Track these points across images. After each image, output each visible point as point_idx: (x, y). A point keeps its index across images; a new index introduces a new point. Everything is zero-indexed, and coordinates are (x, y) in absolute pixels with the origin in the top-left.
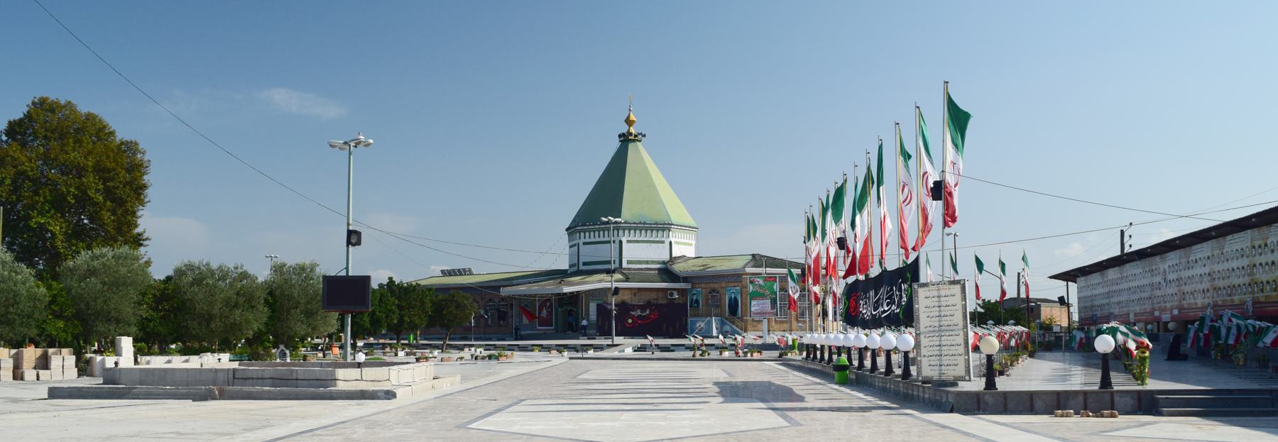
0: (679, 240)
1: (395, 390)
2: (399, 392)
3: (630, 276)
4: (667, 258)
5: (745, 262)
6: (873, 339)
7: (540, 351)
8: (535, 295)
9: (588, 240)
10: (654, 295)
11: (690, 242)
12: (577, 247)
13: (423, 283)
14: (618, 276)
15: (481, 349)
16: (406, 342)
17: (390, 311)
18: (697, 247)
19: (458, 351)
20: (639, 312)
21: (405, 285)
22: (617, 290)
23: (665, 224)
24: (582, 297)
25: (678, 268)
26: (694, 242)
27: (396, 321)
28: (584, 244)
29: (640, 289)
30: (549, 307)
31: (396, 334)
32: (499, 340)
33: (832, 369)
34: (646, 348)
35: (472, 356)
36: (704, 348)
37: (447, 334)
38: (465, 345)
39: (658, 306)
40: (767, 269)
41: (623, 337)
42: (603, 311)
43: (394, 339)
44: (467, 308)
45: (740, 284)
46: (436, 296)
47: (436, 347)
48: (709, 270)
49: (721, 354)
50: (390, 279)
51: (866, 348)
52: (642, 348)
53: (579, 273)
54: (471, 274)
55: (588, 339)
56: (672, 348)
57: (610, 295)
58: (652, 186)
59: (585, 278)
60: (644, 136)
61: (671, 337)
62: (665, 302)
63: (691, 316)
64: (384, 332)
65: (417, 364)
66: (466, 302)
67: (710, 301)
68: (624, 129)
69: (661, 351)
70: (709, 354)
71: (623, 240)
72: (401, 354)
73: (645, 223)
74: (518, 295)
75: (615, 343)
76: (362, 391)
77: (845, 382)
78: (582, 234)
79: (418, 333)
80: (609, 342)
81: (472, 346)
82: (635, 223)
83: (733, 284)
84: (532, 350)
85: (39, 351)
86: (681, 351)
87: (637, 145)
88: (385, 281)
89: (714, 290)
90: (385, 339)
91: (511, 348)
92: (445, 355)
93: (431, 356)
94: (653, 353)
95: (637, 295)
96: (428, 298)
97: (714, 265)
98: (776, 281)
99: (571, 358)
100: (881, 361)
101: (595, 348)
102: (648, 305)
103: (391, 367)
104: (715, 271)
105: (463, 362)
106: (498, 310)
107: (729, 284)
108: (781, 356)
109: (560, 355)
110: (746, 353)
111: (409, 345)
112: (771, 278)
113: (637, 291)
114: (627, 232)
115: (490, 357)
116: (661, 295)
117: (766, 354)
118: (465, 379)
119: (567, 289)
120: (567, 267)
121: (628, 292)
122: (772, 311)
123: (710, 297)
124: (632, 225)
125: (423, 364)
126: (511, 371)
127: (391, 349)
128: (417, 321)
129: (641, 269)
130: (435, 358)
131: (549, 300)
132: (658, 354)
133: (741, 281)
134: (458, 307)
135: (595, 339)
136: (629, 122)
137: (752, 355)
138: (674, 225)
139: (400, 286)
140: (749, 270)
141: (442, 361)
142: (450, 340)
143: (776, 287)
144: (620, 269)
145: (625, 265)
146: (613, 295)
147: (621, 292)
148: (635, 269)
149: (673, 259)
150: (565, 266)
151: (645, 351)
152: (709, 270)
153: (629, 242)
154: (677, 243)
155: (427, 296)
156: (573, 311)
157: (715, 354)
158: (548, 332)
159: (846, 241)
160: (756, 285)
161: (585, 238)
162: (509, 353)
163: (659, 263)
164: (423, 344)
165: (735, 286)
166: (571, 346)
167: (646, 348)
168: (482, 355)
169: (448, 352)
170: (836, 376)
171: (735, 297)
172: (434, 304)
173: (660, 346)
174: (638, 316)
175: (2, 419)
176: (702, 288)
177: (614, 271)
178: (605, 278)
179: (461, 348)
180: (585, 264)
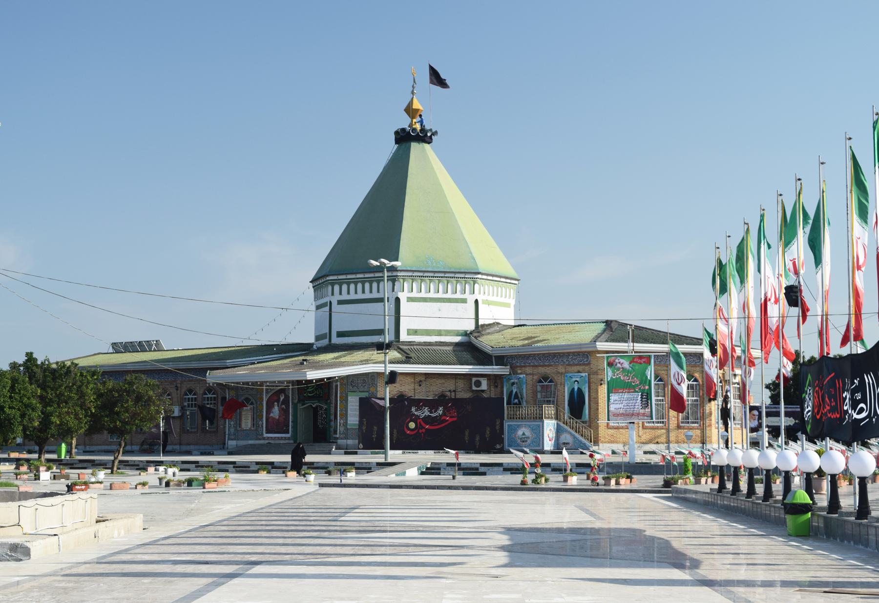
0: (490, 298)
1: (28, 544)
2: (36, 548)
3: (412, 355)
4: (470, 326)
5: (595, 334)
6: (831, 459)
7: (269, 472)
8: (262, 384)
9: (345, 297)
10: (450, 385)
11: (507, 300)
12: (327, 308)
13: (82, 363)
14: (393, 354)
15: (176, 470)
16: (54, 456)
17: (27, 406)
18: (518, 308)
19: (138, 472)
20: (426, 412)
21: (54, 366)
22: (393, 377)
24: (337, 386)
25: (487, 342)
26: (512, 302)
27: (36, 424)
28: (340, 302)
29: (428, 376)
30: (283, 403)
31: (37, 444)
32: (202, 454)
33: (782, 512)
34: (439, 469)
35: (160, 479)
36: (539, 470)
37: (120, 445)
38: (148, 462)
39: (458, 403)
40: (635, 344)
41: (401, 452)
42: (368, 408)
43: (35, 452)
44: (154, 402)
45: (587, 368)
46: (104, 383)
47: (103, 465)
48: (538, 345)
49: (566, 479)
50: (29, 355)
51: (776, 470)
52: (433, 470)
53: (331, 348)
54: (159, 349)
55: (346, 453)
56: (482, 469)
57: (381, 383)
58: (447, 213)
59: (340, 357)
61: (478, 452)
62: (467, 395)
63: (511, 418)
64: (19, 440)
65: (69, 497)
66: (151, 393)
67: (539, 396)
68: (404, 122)
69: (464, 474)
70: (546, 480)
71: (403, 296)
72: (45, 475)
74: (244, 383)
75: (389, 460)
76: (26, 500)
77: (806, 534)
78: (337, 288)
79: (74, 442)
80: (380, 458)
81: (160, 463)
83: (576, 368)
84: (257, 472)
85: (829, 356)
86: (497, 474)
87: (424, 150)
88: (21, 359)
89: (545, 378)
90: (20, 452)
91: (223, 467)
92: (116, 479)
93: (93, 480)
94: (454, 478)
95: (423, 384)
96: (91, 386)
97: (545, 337)
98: (649, 363)
99: (322, 485)
100: (778, 486)
101: (357, 469)
102: (441, 400)
103: (23, 503)
104: (548, 346)
105: (146, 490)
106: (202, 408)
107: (570, 369)
108: (667, 484)
109: (302, 479)
110: (607, 479)
111: (59, 462)
112: (643, 359)
113: (423, 379)
115: (190, 483)
116: (461, 384)
117: (640, 481)
118: (150, 520)
119: (313, 375)
121: (410, 379)
122: (642, 411)
123: (539, 388)
125: (79, 496)
126: (227, 507)
127: (29, 468)
128: (72, 422)
129: (430, 344)
130: (101, 483)
131: (282, 391)
132: (462, 480)
133: (589, 364)
134: (138, 398)
135: (356, 453)
136: (411, 111)
137: (617, 483)
138: (482, 274)
139: (45, 368)
140: (602, 346)
141: (111, 489)
142: (126, 453)
143: (650, 373)
144: (395, 344)
145: (404, 337)
146: (387, 383)
147: (399, 379)
148: (420, 344)
149: (479, 329)
150: (308, 337)
151: (439, 474)
152: (538, 345)
153: (410, 299)
154: (488, 303)
155: (88, 383)
156: (321, 408)
157: (555, 479)
158: (272, 442)
159: (801, 291)
160: (618, 369)
161: (340, 293)
162: (221, 475)
163: (457, 333)
164: (81, 461)
165: (579, 372)
166: (319, 465)
167: (439, 469)
168: (176, 478)
169: (122, 473)
170: (787, 520)
171: (579, 390)
172: (100, 395)
173: (462, 466)
174: (425, 417)
176: (527, 375)
177: (389, 346)
178: (373, 357)
179: (142, 467)
180: (340, 334)
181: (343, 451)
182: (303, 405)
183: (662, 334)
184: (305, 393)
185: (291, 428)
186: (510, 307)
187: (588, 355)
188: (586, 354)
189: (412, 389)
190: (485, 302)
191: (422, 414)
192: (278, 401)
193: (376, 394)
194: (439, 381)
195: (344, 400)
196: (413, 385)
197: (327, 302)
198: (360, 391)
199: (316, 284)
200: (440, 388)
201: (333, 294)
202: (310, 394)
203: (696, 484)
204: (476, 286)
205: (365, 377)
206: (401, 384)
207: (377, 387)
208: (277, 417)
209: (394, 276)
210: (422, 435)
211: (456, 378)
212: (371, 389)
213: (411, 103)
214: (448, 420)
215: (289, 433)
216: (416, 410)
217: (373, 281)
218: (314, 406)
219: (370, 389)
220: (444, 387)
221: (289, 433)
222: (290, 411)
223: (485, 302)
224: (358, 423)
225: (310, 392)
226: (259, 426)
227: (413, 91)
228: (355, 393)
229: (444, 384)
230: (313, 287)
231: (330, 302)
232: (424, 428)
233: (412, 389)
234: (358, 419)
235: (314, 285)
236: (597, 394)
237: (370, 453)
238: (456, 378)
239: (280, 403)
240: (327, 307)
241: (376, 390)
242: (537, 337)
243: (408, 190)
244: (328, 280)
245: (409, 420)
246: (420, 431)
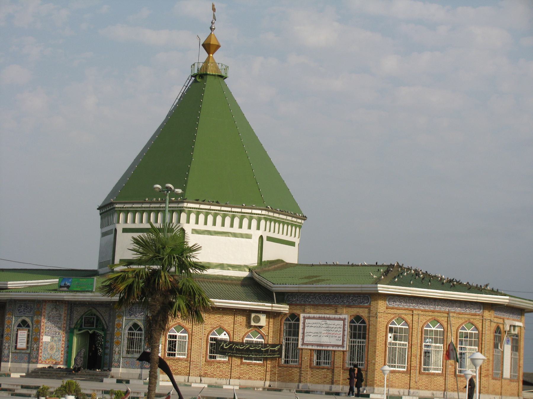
12: (113, 235)
181: (99, 381)
186: (294, 246)
187: (369, 297)
188: (367, 295)
190: (269, 239)
197: (113, 229)
199: (103, 211)
217: (144, 211)
223: (269, 239)
226: (34, 349)
230: (101, 214)
231: (116, 230)
235: (102, 212)
236: (376, 336)
242: (319, 276)
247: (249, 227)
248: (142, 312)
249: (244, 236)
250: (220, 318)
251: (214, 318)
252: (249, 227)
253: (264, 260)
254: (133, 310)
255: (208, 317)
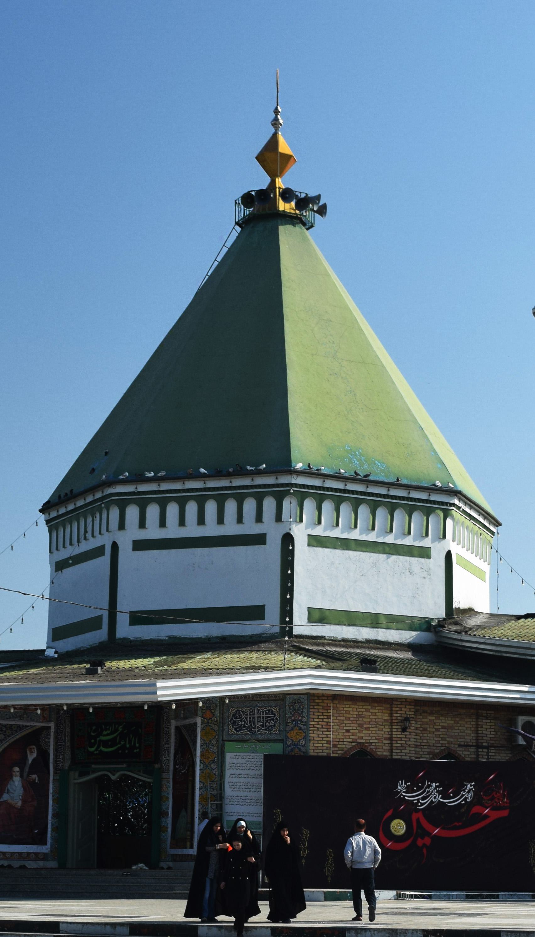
12: (105, 560)
18: (495, 589)
23: (433, 489)
60: (322, 211)
73: (366, 480)
78: (132, 512)
82: (337, 477)
87: (305, 238)
114: (309, 505)
120: (42, 645)
124: (330, 484)
129: (355, 643)
158: (30, 864)
161: (142, 524)
175: (534, 641)
182: (82, 775)
183: (384, 699)
184: (92, 746)
185: (53, 830)
189: (386, 739)
191: (423, 799)
192: (22, 763)
193: (305, 746)
194: (443, 722)
195: (213, 761)
196: (387, 729)
198: (259, 741)
200: (443, 739)
201: (122, 526)
202: (105, 747)
203: (397, 899)
204: (449, 521)
205: (272, 703)
206: (361, 725)
207: (308, 729)
208: (19, 804)
209: (282, 485)
210: (425, 851)
211: (478, 716)
212: (292, 735)
213: (273, 143)
214: (486, 816)
215: (46, 844)
216: (409, 790)
217: (226, 496)
218: (113, 778)
219: (289, 735)
220: (451, 737)
221: (46, 844)
222: (51, 791)
224: (261, 819)
225: (106, 744)
227: (276, 119)
228: (246, 745)
229: (452, 728)
230: (48, 522)
231: (115, 546)
232: (429, 834)
233: (386, 739)
234: (260, 809)
237: (322, 897)
238: (478, 716)
239: (27, 769)
240: (102, 558)
241: (306, 738)
243: (287, 311)
244: (112, 495)
245: (390, 813)
246: (420, 842)
247: (259, 518)
248: (270, 720)
249: (416, 553)
250: (446, 730)
251: (434, 730)
252: (259, 518)
253: (226, 744)
254: (243, 716)
255: (421, 729)
